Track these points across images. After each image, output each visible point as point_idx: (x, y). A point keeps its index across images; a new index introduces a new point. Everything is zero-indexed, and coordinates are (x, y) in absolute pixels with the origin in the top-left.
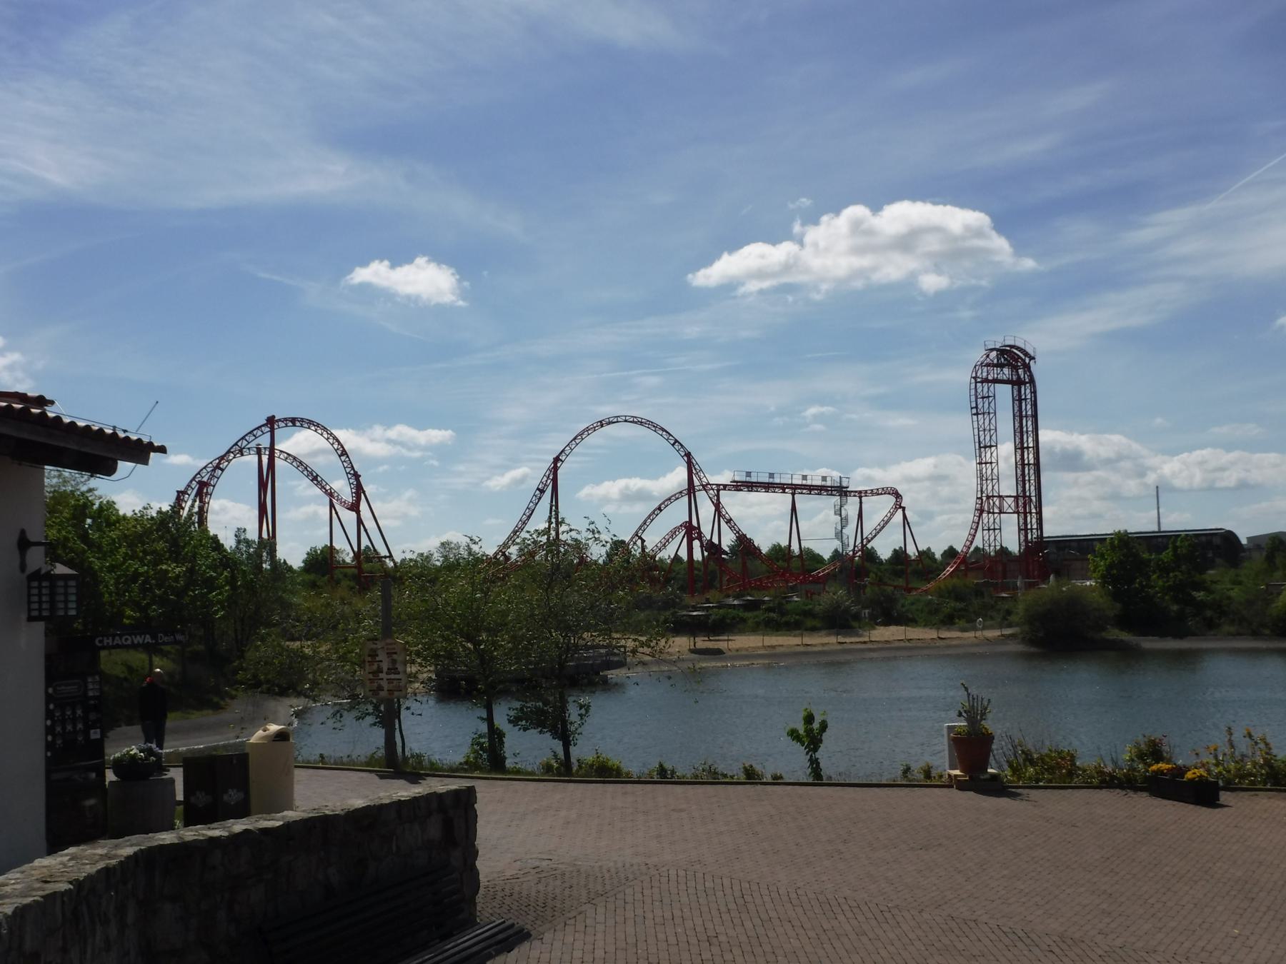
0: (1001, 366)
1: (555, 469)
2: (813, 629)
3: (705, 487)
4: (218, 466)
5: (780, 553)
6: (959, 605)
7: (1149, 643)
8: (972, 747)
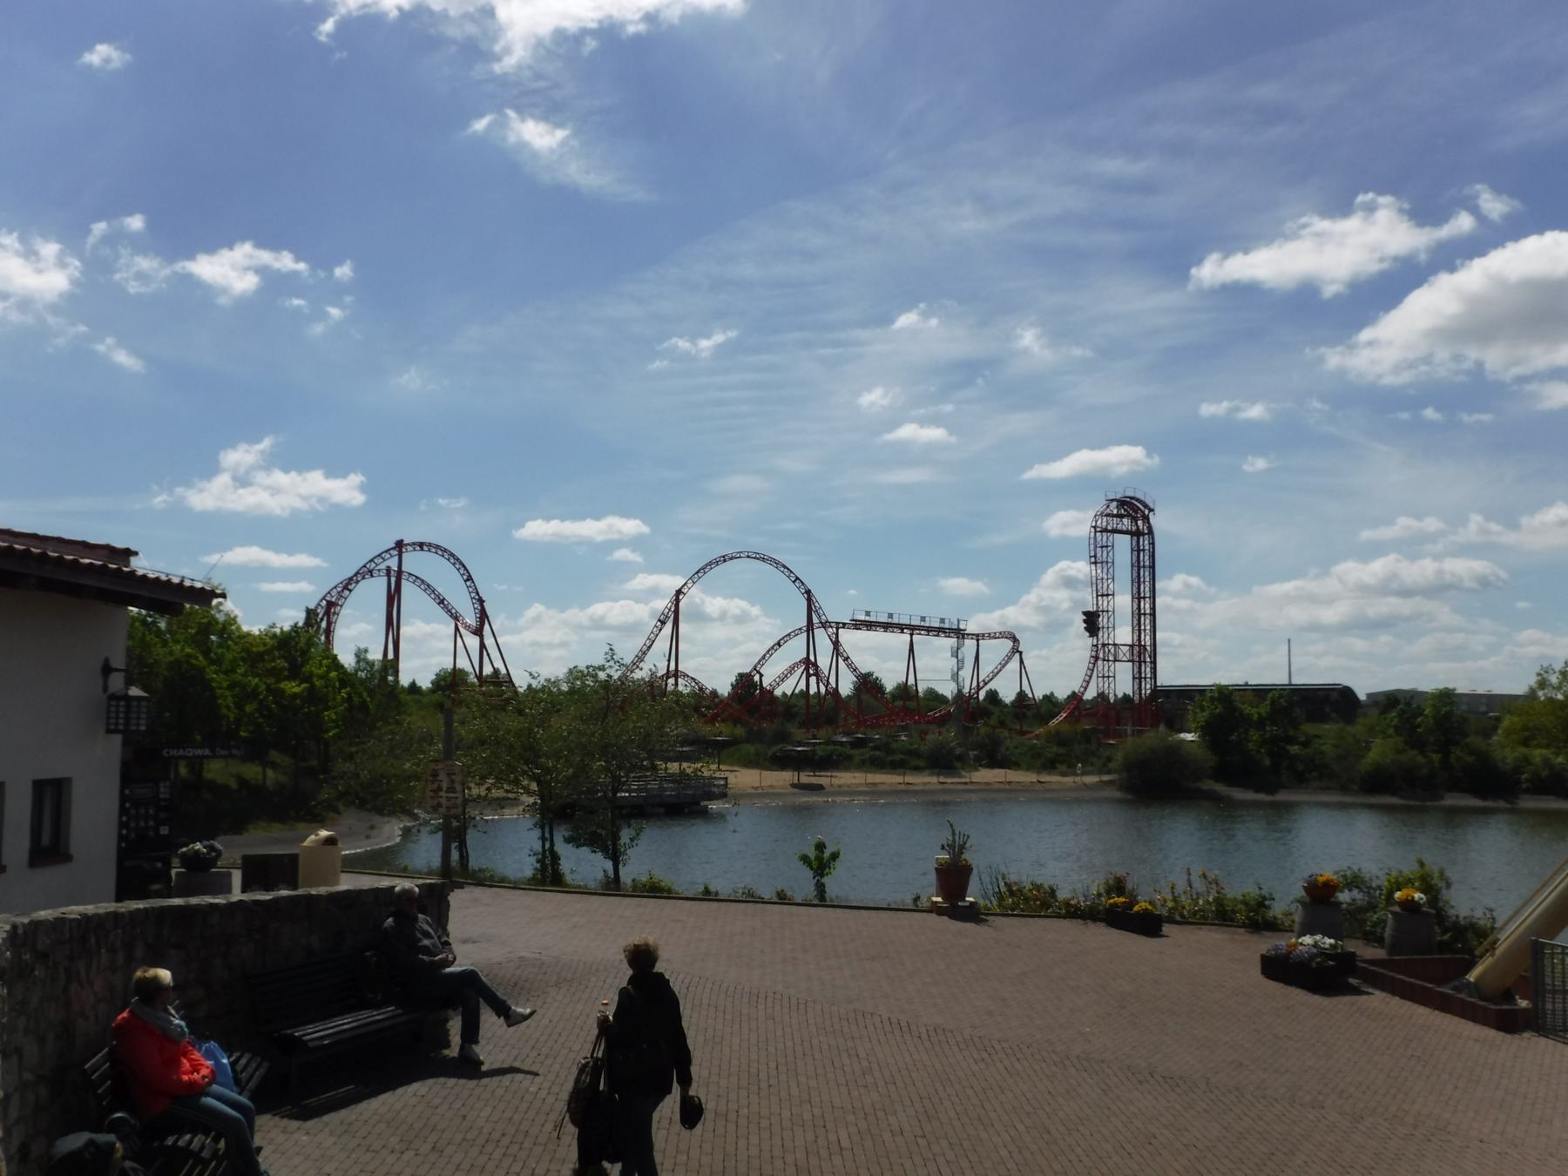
0: (1121, 516)
1: (677, 601)
2: (917, 769)
3: (825, 625)
4: (348, 585)
5: (905, 691)
6: (1061, 750)
7: (1239, 794)
8: (953, 877)
